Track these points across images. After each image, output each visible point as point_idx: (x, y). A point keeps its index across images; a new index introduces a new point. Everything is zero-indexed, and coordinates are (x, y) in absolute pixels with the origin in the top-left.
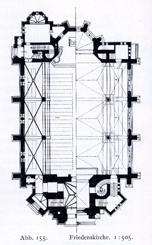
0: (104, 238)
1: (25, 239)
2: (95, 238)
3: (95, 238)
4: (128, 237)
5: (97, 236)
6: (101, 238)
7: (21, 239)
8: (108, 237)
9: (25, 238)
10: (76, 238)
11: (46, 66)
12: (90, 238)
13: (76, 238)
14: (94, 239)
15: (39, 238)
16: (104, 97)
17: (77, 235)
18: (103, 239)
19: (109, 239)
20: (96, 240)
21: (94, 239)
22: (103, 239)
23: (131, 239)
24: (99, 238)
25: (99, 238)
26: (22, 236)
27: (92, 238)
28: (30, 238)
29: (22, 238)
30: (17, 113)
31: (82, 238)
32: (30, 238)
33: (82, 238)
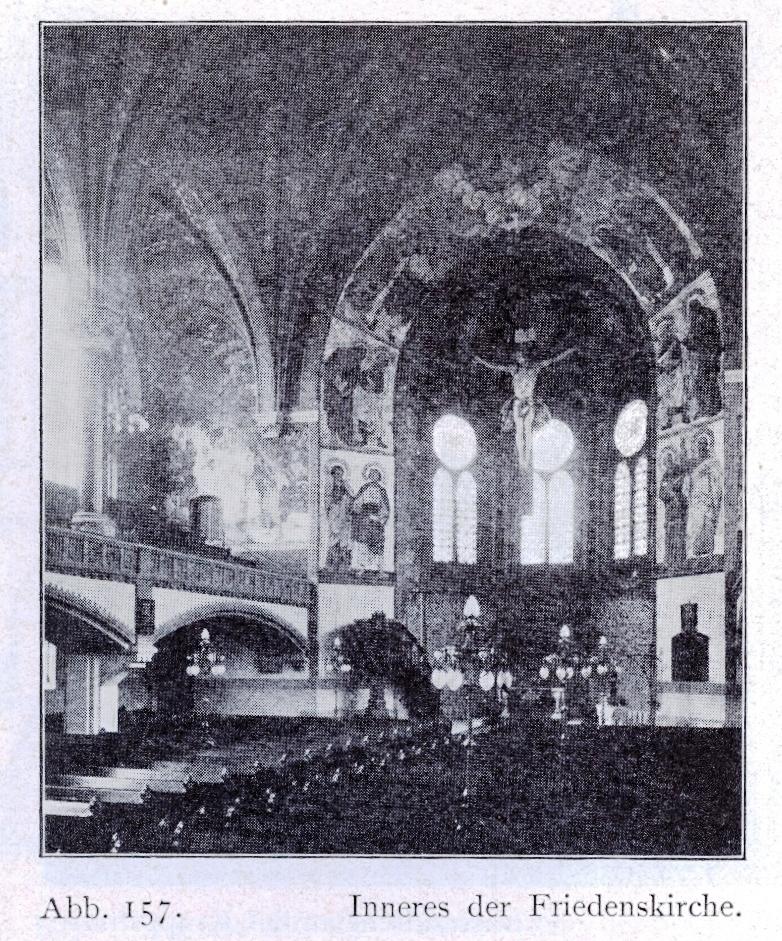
0: (710, 907)
1: (64, 912)
2: (665, 909)
3: (665, 909)
4: (587, 906)
5: (674, 901)
6: (696, 909)
7: (45, 917)
8: (731, 906)
9: (64, 911)
10: (561, 909)
11: (44, 668)
12: (636, 910)
13: (561, 909)
14: (656, 913)
15: (137, 908)
16: (274, 661)
17: (567, 896)
18: (366, 915)
19: (735, 915)
20: (667, 919)
21: (656, 913)
22: (366, 915)
23: (101, 914)
24: (685, 909)
25: (685, 909)
26: (52, 901)
27: (649, 907)
28: (92, 911)
29: (52, 907)
30: (754, 703)
31: (595, 909)
32: (92, 911)
33: (595, 909)
